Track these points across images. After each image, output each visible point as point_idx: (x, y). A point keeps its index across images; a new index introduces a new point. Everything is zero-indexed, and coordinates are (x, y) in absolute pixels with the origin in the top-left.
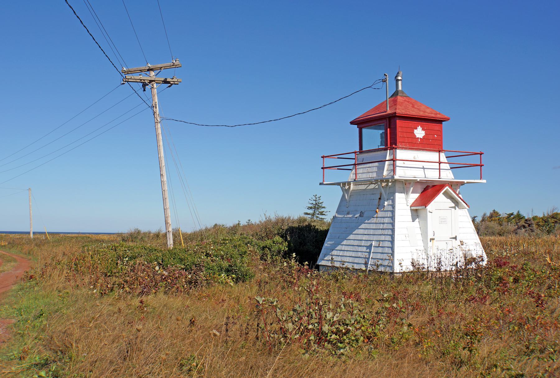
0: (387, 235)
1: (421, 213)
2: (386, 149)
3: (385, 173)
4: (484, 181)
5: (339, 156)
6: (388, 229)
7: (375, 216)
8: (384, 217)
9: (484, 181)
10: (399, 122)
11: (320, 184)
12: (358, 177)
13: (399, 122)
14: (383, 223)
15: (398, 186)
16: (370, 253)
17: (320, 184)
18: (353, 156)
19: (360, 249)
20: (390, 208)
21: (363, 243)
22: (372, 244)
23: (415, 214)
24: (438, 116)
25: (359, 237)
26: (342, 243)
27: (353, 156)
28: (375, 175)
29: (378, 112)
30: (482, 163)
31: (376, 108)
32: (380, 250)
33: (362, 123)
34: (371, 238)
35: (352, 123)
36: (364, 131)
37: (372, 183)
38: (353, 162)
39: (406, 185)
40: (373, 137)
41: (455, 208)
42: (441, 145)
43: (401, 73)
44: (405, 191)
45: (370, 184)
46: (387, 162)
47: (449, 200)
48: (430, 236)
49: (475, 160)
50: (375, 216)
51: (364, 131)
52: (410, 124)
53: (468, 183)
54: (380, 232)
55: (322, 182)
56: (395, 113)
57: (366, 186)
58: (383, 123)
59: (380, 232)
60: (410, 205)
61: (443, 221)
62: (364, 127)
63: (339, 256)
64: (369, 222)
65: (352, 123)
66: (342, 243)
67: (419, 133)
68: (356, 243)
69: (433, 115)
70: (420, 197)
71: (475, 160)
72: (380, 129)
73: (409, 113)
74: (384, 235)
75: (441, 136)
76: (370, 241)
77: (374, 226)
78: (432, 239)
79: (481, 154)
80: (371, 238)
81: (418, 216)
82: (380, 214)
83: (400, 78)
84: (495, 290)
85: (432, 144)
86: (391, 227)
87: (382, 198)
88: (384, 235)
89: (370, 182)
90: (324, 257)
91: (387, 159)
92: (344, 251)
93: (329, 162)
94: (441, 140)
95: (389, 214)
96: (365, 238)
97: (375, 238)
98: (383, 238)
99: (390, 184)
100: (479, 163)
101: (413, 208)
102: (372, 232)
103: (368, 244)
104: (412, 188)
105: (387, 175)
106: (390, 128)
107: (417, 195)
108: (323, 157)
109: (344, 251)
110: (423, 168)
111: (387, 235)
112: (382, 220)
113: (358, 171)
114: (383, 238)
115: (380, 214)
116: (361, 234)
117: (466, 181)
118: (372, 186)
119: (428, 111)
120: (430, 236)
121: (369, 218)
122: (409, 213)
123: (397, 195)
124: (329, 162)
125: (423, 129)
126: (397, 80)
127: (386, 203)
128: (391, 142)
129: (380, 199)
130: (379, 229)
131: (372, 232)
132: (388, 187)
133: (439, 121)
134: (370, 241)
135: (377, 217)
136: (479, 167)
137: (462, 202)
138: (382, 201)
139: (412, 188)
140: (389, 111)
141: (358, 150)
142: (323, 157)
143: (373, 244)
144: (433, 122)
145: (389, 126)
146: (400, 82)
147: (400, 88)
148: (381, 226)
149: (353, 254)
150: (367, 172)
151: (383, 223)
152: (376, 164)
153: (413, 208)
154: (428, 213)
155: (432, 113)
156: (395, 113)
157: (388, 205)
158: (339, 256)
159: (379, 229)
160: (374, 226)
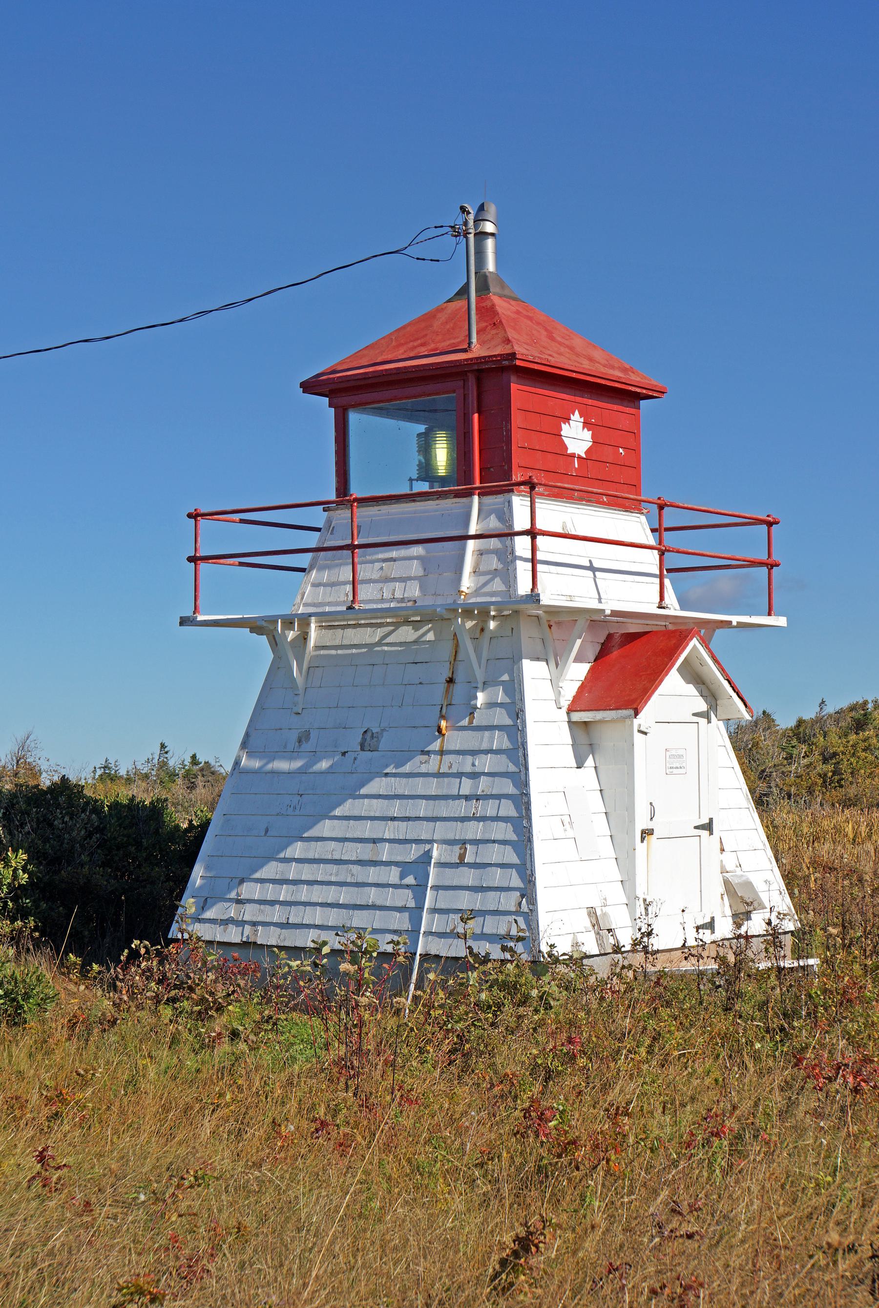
0: (497, 819)
1: (608, 737)
2: (469, 494)
3: (467, 583)
4: (781, 621)
5: (245, 516)
6: (498, 797)
7: (436, 746)
8: (474, 753)
9: (781, 621)
10: (520, 393)
11: (184, 621)
12: (362, 595)
13: (520, 393)
14: (474, 776)
15: (528, 634)
16: (419, 890)
17: (184, 621)
18: (317, 516)
19: (373, 874)
20: (501, 717)
21: (385, 853)
22: (428, 855)
23: (585, 741)
24: (634, 378)
25: (367, 830)
26: (288, 853)
27: (317, 516)
28: (414, 591)
29: (444, 345)
30: (775, 557)
31: (402, 335)
32: (469, 877)
33: (346, 391)
34: (423, 831)
35: (308, 387)
36: (354, 418)
37: (407, 622)
38: (312, 540)
39: (556, 626)
40: (399, 448)
41: (706, 715)
42: (635, 487)
43: (491, 211)
44: (553, 656)
45: (397, 625)
46: (471, 544)
47: (691, 689)
48: (642, 823)
49: (751, 543)
50: (436, 746)
51: (354, 418)
52: (551, 403)
53: (741, 625)
54: (461, 808)
55: (189, 613)
56: (513, 356)
57: (380, 632)
58: (446, 399)
59: (461, 808)
60: (565, 703)
61: (674, 764)
62: (356, 406)
63: (272, 903)
64: (407, 768)
65: (308, 387)
66: (288, 853)
67: (577, 437)
68: (352, 851)
69: (617, 374)
70: (591, 670)
71: (751, 543)
72: (417, 421)
73: (552, 361)
74: (483, 819)
75: (634, 450)
76: (418, 841)
77: (433, 787)
78: (647, 833)
79: (770, 524)
80: (423, 831)
81: (592, 748)
82: (455, 740)
83: (489, 227)
84: (549, 983)
85: (607, 481)
86: (510, 788)
87: (459, 677)
88: (483, 819)
89: (403, 616)
90: (203, 908)
91: (472, 531)
92: (296, 882)
93: (216, 537)
94: (636, 468)
95: (499, 740)
96: (390, 831)
97: (441, 830)
98: (475, 830)
99: (492, 625)
100: (764, 557)
101: (577, 717)
102: (422, 808)
103: (413, 853)
104: (579, 642)
105: (477, 592)
106: (480, 413)
107: (578, 672)
108: (194, 516)
109: (296, 882)
110: (591, 568)
111: (497, 819)
112: (466, 764)
113: (364, 572)
114: (475, 830)
115: (455, 740)
116: (376, 813)
117: (735, 619)
118: (406, 634)
119: (597, 355)
120: (642, 823)
121: (403, 755)
122: (565, 735)
123: (526, 663)
124: (216, 537)
125: (587, 425)
126: (482, 236)
127: (481, 698)
128: (489, 467)
129: (451, 681)
130: (458, 797)
131: (422, 808)
132: (487, 635)
133: (629, 397)
134: (418, 841)
135: (442, 752)
136: (765, 570)
137: (734, 695)
138: (459, 689)
139: (579, 642)
140: (478, 350)
141: (333, 497)
142: (194, 516)
143: (435, 854)
144: (613, 395)
145: (477, 405)
146: (490, 243)
147: (491, 266)
148: (467, 786)
149: (344, 896)
150: (393, 580)
151: (474, 776)
152: (418, 550)
153: (577, 717)
154: (637, 737)
155: (612, 367)
156: (513, 356)
157: (491, 705)
158: (272, 903)
159: (458, 797)
160: (433, 787)
